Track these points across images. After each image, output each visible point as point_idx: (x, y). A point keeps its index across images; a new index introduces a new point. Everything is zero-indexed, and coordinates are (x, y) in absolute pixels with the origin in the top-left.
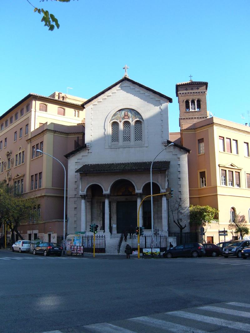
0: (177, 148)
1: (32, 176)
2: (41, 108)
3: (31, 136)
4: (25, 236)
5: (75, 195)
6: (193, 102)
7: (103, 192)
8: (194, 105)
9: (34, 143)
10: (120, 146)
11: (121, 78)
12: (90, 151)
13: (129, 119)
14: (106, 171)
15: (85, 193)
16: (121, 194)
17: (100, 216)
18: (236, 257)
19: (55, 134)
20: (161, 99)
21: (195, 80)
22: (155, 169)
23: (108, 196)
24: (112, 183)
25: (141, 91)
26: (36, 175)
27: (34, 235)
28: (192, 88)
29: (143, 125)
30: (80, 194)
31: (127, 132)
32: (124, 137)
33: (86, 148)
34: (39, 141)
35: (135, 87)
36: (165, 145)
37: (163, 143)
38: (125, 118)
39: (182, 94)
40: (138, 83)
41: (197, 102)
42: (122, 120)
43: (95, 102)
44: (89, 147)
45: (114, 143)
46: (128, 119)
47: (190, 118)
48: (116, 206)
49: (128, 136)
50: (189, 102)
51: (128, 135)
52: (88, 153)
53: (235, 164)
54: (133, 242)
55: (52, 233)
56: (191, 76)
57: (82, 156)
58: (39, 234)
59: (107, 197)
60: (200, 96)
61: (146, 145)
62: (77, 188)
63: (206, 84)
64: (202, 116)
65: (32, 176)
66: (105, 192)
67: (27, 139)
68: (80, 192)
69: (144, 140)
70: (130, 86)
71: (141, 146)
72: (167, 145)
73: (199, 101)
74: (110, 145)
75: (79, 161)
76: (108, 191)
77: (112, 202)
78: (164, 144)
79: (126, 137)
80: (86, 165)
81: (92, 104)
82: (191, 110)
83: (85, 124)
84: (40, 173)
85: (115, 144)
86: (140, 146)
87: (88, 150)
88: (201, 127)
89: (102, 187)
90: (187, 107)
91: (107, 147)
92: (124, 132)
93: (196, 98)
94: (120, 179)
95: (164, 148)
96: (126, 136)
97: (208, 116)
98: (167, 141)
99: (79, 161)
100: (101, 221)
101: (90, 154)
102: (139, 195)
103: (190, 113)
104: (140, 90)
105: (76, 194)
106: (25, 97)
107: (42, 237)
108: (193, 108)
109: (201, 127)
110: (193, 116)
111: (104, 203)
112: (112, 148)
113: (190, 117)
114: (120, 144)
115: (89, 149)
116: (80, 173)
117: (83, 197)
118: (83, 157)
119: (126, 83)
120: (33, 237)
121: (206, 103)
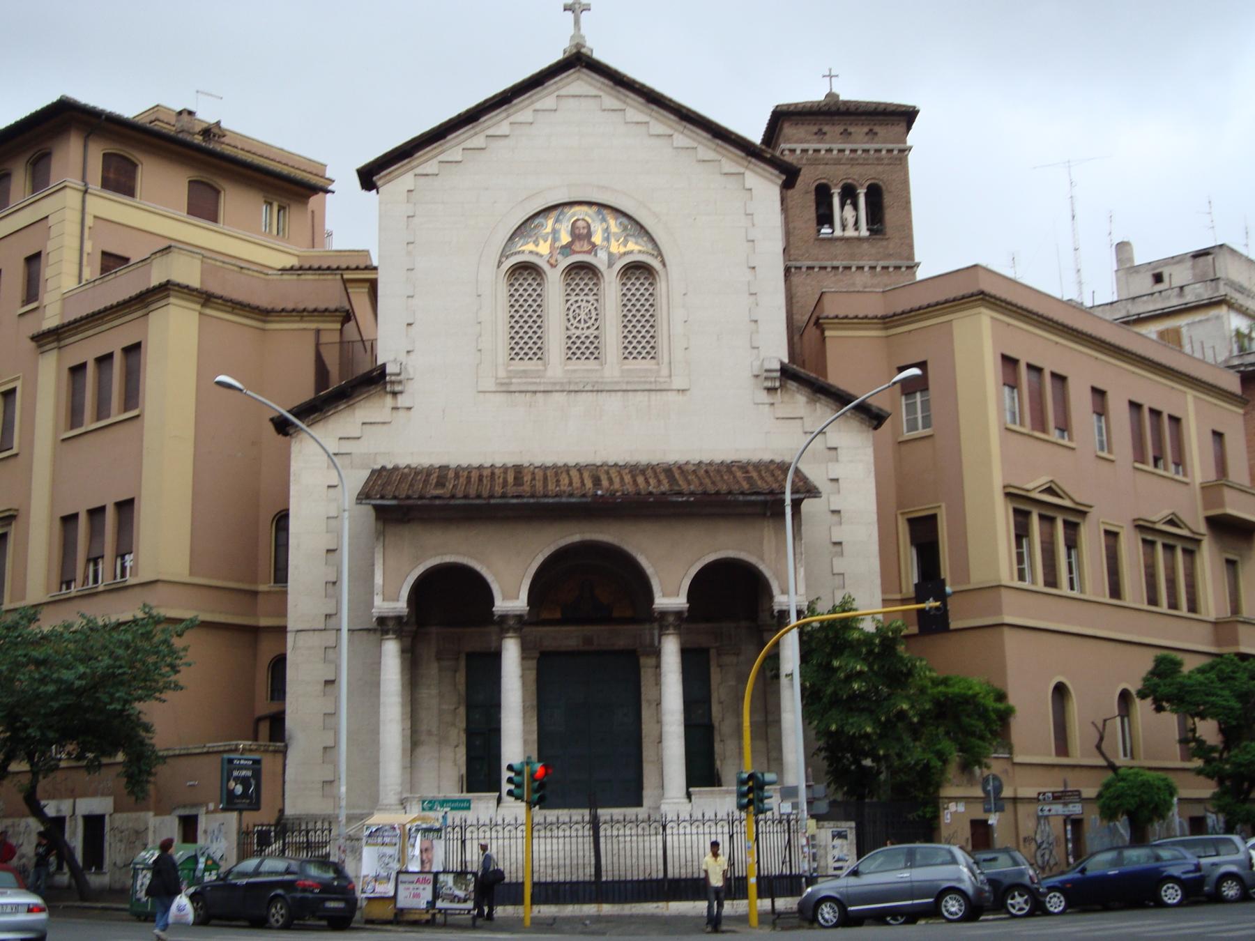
0: (822, 397)
1: (69, 520)
2: (112, 176)
3: (62, 314)
4: (22, 829)
5: (328, 616)
6: (849, 193)
7: (492, 603)
8: (855, 206)
9: (86, 350)
10: (555, 384)
11: (557, 56)
12: (402, 401)
13: (596, 255)
14: (515, 501)
15: (401, 606)
16: (558, 615)
17: (453, 724)
18: (449, 912)
19: (208, 311)
20: (747, 168)
21: (850, 92)
22: (753, 498)
23: (519, 624)
24: (540, 559)
25: (653, 123)
26: (96, 513)
27: (80, 823)
28: (820, 130)
29: (661, 286)
30: (376, 612)
31: (583, 316)
32: (569, 337)
33: (385, 383)
34: (113, 340)
35: (625, 102)
36: (769, 384)
37: (757, 376)
38: (577, 247)
39: (798, 152)
40: (643, 86)
41: (867, 195)
42: (560, 258)
43: (428, 162)
44: (400, 382)
45: (518, 365)
46: (589, 252)
47: (835, 268)
48: (534, 672)
49: (587, 337)
50: (831, 196)
51: (587, 333)
52: (395, 408)
53: (1065, 484)
54: (535, 855)
55: (207, 812)
56: (831, 76)
57: (364, 424)
58: (118, 816)
59: (515, 630)
60: (880, 168)
61: (677, 383)
62: (334, 583)
63: (907, 116)
64: (891, 263)
65: (69, 520)
66: (502, 605)
67: (35, 331)
68: (378, 600)
69: (666, 359)
70: (600, 97)
71: (653, 387)
72: (777, 384)
73: (875, 196)
74: (502, 373)
75: (346, 447)
76: (518, 598)
77: (713, 652)
78: (766, 378)
79: (578, 337)
80: (383, 468)
81: (412, 168)
82: (838, 233)
83: (380, 270)
84: (126, 507)
85: (524, 371)
86: (647, 387)
87: (395, 394)
88: (111, 328)
89: (490, 578)
90: (825, 218)
91: (489, 384)
92: (571, 316)
93: (862, 177)
94: (576, 538)
95: (763, 396)
96: (578, 333)
97: (917, 260)
98: (778, 367)
99: (346, 447)
100: (457, 746)
101: (401, 413)
102: (671, 619)
103: (838, 243)
104: (646, 119)
105: (329, 612)
106: (33, 111)
107: (137, 833)
108: (851, 221)
109: (111, 328)
110: (852, 257)
111: (494, 659)
112: (512, 388)
113: (836, 263)
114: (550, 373)
115: (397, 388)
116: (376, 507)
117: (384, 626)
118: (368, 427)
119: (579, 82)
120: (74, 833)
121: (908, 202)
